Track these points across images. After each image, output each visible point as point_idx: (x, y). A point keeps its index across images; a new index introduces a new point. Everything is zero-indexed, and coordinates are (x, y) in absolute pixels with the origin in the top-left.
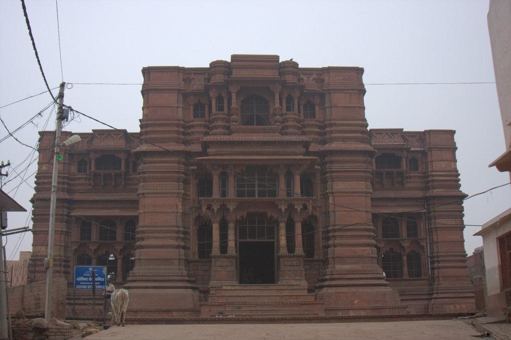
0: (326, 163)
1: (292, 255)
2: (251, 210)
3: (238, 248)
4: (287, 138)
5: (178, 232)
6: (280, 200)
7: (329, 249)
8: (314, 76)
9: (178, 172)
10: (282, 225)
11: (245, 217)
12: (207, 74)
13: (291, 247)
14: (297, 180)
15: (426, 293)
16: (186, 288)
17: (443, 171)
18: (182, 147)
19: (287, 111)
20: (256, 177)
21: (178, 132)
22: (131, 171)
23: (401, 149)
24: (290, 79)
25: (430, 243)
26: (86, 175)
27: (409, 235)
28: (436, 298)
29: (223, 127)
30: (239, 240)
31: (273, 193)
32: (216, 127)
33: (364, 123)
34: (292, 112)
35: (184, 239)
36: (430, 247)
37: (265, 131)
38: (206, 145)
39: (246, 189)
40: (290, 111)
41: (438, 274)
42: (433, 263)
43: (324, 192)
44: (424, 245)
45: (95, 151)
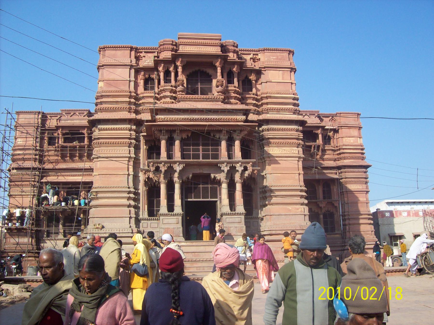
4: (228, 107)
5: (129, 192)
9: (130, 139)
10: (224, 186)
11: (190, 178)
12: (156, 52)
14: (237, 144)
15: (339, 245)
17: (352, 146)
18: (133, 116)
21: (130, 103)
22: (144, 213)
23: (318, 128)
25: (342, 204)
26: (56, 148)
27: (324, 198)
29: (172, 97)
30: (219, 147)
31: (216, 156)
32: (165, 97)
35: (135, 200)
36: (342, 206)
37: (207, 100)
38: (156, 112)
41: (349, 229)
42: (344, 220)
44: (338, 205)
45: (63, 127)
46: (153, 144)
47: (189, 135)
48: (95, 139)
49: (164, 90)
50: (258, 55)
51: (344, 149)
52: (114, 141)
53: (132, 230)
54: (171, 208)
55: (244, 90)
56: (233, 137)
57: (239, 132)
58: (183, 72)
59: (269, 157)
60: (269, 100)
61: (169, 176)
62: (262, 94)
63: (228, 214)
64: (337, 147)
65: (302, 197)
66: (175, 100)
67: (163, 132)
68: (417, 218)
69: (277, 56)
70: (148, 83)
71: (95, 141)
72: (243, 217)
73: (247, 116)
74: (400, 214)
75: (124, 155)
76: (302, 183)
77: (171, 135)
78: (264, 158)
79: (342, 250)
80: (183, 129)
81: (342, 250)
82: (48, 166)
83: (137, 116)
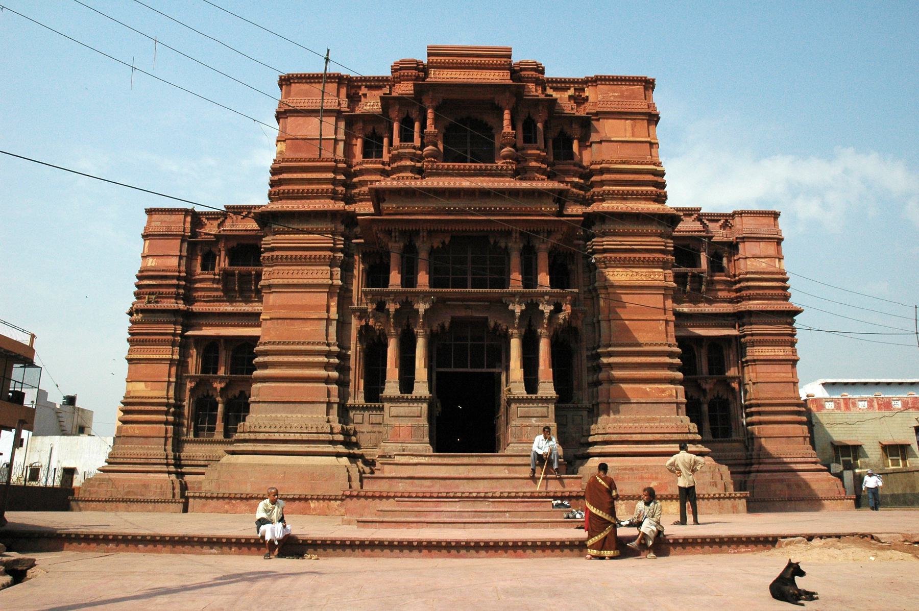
0: (594, 236)
1: (534, 396)
2: (462, 313)
3: (434, 382)
5: (328, 354)
6: (513, 295)
7: (600, 387)
8: (571, 92)
13: (531, 383)
14: (543, 261)
16: (338, 455)
19: (525, 142)
20: (470, 256)
21: (334, 182)
24: (533, 90)
27: (711, 372)
28: (758, 471)
29: (413, 169)
33: (659, 169)
34: (534, 145)
39: (451, 277)
40: (531, 142)
43: (591, 288)
46: (378, 262)
47: (447, 242)
48: (267, 250)
49: (399, 157)
50: (583, 90)
51: (748, 280)
52: (302, 258)
53: (332, 428)
54: (407, 383)
55: (556, 157)
56: (533, 247)
57: (546, 235)
58: (436, 120)
59: (606, 288)
60: (606, 177)
61: (405, 322)
62: (591, 164)
63: (363, 409)
64: (735, 276)
65: (671, 367)
66: (419, 174)
67: (393, 234)
68: (887, 413)
69: (622, 92)
70: (372, 148)
71: (266, 254)
72: (552, 407)
73: (562, 207)
74: (854, 404)
75: (320, 281)
76: (673, 341)
77: (410, 242)
78: (595, 289)
79: (744, 473)
80: (433, 230)
81: (744, 473)
82: (197, 307)
83: (347, 207)
